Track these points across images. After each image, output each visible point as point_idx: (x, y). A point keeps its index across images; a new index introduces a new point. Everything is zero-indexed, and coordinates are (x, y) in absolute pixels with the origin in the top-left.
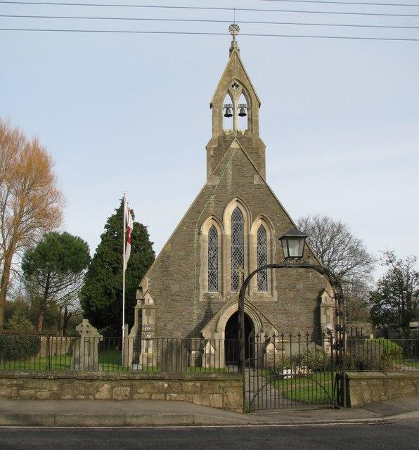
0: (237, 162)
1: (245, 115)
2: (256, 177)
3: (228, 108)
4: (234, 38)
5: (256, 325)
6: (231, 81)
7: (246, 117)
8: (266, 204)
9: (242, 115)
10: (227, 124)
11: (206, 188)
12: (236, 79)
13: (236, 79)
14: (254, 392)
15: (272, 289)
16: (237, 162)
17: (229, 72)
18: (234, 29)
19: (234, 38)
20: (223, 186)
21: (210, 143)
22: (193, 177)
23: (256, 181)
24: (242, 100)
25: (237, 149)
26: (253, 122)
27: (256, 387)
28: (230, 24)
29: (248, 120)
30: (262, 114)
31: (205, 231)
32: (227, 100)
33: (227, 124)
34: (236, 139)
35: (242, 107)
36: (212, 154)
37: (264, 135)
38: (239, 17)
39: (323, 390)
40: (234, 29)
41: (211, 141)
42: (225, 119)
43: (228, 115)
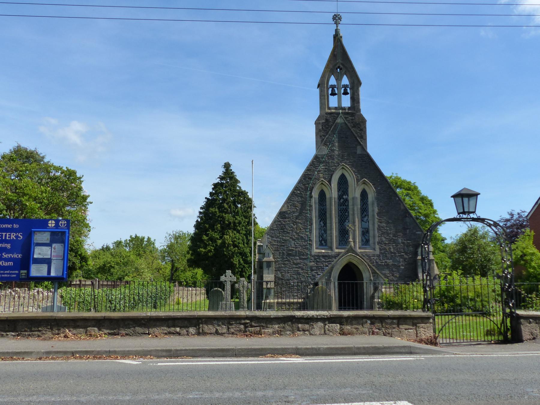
0: (342, 133)
1: (348, 94)
2: (359, 148)
3: (333, 87)
4: (337, 27)
5: (364, 275)
6: (336, 65)
7: (349, 96)
8: (368, 167)
9: (346, 93)
10: (333, 102)
11: (316, 157)
12: (340, 61)
13: (340, 61)
14: (453, 339)
15: (374, 243)
16: (342, 133)
17: (334, 55)
18: (337, 19)
19: (337, 27)
20: (330, 156)
21: (318, 119)
22: (301, 140)
23: (359, 151)
24: (345, 81)
25: (341, 124)
26: (355, 100)
27: (451, 325)
28: (333, 14)
29: (351, 98)
30: (363, 91)
31: (315, 194)
32: (333, 81)
33: (333, 102)
34: (341, 115)
35: (345, 87)
36: (321, 128)
37: (365, 109)
38: (341, 8)
39: (492, 323)
40: (337, 19)
41: (319, 117)
42: (331, 97)
43: (333, 94)
